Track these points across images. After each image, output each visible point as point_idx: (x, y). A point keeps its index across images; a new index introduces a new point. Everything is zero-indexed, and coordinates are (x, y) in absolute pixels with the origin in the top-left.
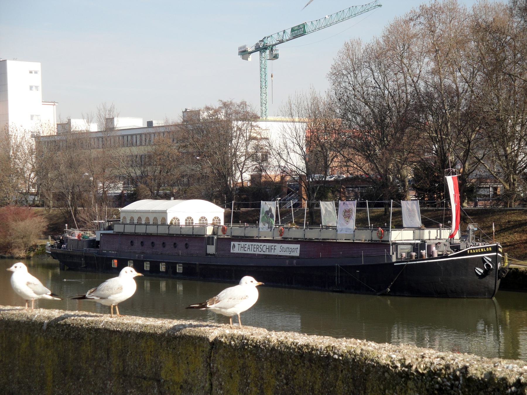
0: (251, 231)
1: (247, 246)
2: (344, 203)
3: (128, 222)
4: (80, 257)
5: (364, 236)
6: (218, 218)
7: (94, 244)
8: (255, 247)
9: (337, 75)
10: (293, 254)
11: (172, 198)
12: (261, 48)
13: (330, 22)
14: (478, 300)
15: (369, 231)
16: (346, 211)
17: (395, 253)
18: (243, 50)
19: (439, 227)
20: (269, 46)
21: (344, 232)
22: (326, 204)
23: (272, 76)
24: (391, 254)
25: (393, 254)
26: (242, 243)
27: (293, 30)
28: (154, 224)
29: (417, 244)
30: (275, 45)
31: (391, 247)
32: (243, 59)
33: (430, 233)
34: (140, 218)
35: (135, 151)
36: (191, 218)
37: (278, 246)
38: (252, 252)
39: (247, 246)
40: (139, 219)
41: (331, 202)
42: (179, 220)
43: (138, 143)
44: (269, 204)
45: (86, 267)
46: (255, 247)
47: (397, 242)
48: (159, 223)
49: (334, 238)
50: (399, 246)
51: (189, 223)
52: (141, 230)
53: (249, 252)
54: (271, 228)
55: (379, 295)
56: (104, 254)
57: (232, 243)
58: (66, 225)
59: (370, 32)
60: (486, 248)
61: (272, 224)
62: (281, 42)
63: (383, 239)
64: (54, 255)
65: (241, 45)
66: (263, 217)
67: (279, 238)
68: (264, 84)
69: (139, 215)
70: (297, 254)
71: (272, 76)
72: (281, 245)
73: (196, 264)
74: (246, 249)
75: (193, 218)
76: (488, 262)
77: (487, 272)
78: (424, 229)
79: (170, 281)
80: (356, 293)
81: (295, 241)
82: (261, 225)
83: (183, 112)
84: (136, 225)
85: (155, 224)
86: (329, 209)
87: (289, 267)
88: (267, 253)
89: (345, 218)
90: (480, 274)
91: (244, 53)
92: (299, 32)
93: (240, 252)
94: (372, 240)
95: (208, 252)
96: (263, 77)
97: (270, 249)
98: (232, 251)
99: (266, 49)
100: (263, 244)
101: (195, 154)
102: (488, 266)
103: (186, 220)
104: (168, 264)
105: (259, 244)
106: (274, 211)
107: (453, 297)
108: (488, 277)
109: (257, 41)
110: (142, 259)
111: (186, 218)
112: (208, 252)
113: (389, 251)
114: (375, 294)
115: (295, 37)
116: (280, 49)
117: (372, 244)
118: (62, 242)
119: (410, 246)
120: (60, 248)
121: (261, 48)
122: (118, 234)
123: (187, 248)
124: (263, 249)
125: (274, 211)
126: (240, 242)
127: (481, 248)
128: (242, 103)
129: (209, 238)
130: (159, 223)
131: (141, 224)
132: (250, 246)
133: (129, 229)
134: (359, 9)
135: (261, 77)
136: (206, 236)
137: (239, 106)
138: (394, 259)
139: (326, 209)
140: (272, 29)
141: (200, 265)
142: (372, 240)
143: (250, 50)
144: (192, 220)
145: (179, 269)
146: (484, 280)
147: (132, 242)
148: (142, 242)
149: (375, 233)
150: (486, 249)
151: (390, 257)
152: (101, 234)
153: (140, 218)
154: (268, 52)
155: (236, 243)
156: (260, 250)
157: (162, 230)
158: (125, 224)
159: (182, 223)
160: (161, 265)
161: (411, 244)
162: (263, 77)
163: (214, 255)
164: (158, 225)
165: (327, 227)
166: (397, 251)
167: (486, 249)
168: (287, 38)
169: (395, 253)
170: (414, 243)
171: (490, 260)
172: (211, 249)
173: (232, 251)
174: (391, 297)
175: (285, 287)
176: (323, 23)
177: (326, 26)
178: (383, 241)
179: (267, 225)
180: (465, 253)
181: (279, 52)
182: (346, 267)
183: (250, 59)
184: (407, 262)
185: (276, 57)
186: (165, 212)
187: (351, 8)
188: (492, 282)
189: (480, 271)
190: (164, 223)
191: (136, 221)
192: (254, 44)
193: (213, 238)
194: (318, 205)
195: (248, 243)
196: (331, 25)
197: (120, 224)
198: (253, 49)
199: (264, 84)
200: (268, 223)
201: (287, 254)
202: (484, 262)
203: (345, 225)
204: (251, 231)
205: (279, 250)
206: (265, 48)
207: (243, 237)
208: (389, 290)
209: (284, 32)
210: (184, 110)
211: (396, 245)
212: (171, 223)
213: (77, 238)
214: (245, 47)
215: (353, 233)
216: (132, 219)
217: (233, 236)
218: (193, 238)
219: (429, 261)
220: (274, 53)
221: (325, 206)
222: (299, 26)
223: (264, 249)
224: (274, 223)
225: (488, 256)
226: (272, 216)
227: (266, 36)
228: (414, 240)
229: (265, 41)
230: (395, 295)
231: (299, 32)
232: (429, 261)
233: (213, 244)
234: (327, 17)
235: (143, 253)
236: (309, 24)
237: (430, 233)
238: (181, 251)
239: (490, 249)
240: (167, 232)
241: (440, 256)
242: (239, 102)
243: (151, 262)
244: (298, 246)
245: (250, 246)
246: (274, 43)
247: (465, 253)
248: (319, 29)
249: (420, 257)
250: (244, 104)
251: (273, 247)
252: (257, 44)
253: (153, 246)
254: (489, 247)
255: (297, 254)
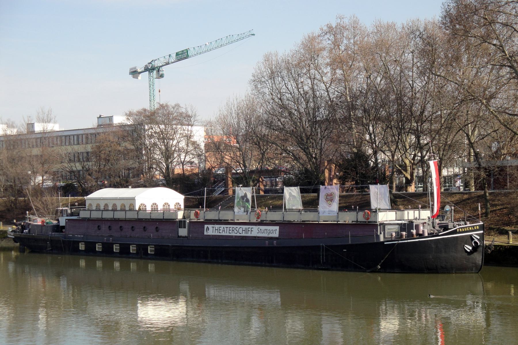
0: (226, 215)
1: (221, 229)
2: (325, 188)
3: (94, 208)
4: (45, 241)
5: (348, 217)
6: (179, 203)
7: (58, 228)
8: (250, 229)
9: (257, 81)
10: (271, 235)
11: (130, 187)
12: (150, 69)
13: (210, 48)
14: (467, 275)
15: (355, 213)
16: (328, 195)
17: (382, 233)
18: (134, 70)
19: (418, 208)
20: (157, 67)
21: (326, 214)
22: (290, 190)
23: (159, 92)
24: (379, 234)
25: (381, 233)
26: (217, 226)
27: (177, 54)
28: (121, 210)
29: (405, 224)
30: (162, 66)
31: (379, 227)
32: (134, 77)
33: (408, 213)
34: (106, 205)
35: (80, 148)
36: (156, 204)
37: (255, 228)
38: (228, 234)
39: (221, 229)
40: (106, 205)
41: (296, 188)
42: (145, 206)
43: (84, 141)
44: (244, 190)
45: (52, 250)
46: (231, 229)
47: (385, 222)
48: (127, 208)
49: (315, 220)
50: (386, 226)
51: (155, 208)
52: (108, 215)
53: (223, 234)
54: (247, 212)
55: (369, 272)
56: (70, 237)
57: (206, 226)
58: (28, 212)
59: (286, 45)
60: (473, 227)
61: (248, 207)
62: (168, 64)
63: (369, 220)
64: (15, 240)
65: (132, 66)
66: (238, 202)
67: (254, 220)
68: (152, 98)
69: (106, 202)
70: (276, 235)
71: (159, 92)
72: (259, 227)
73: (168, 246)
74: (220, 231)
75: (157, 204)
76: (476, 240)
77: (475, 248)
78: (403, 211)
79: (142, 262)
80: (343, 271)
81: (273, 223)
82: (236, 209)
83: (98, 118)
84: (103, 211)
85: (123, 210)
86: (293, 194)
87: (269, 247)
88: (244, 234)
89: (327, 201)
90: (469, 251)
91: (135, 73)
92: (182, 55)
93: (214, 234)
94: (357, 221)
95: (180, 234)
96: (152, 92)
97: (246, 231)
98: (205, 233)
99: (154, 69)
100: (239, 226)
101: (119, 152)
102: (475, 243)
103: (152, 206)
104: (87, 244)
105: (235, 226)
106: (249, 196)
107: (443, 273)
108: (475, 254)
109: (146, 64)
110: (111, 241)
111: (163, 203)
112: (180, 234)
113: (377, 231)
114: (365, 271)
115: (179, 60)
116: (165, 70)
117: (357, 225)
118: (23, 227)
119: (397, 226)
120: (22, 232)
121: (150, 69)
122: (84, 220)
123: (157, 231)
124: (239, 231)
125: (249, 196)
126: (214, 225)
127: (469, 227)
128: (176, 105)
129: (180, 221)
130: (127, 208)
131: (108, 210)
132: (226, 229)
133: (96, 215)
134: (236, 37)
135: (150, 92)
136: (177, 220)
137: (173, 108)
138: (382, 239)
139: (290, 194)
140: (157, 55)
141: (173, 246)
142: (357, 221)
143: (139, 71)
144: (157, 206)
145: (98, 247)
146: (472, 256)
147: (99, 226)
148: (110, 227)
149: (361, 214)
150: (474, 228)
151: (378, 237)
152: (66, 219)
153: (106, 205)
154: (155, 72)
155: (210, 226)
156: (236, 232)
157: (131, 215)
158: (91, 211)
159: (149, 208)
160: (131, 247)
161: (398, 224)
162: (152, 92)
163: (186, 237)
164: (126, 211)
165: (291, 210)
166: (384, 230)
167: (474, 228)
168: (173, 61)
169: (382, 233)
170: (401, 224)
171: (478, 237)
172: (183, 232)
173: (205, 233)
174: (382, 274)
175: (265, 266)
176: (204, 48)
177: (208, 51)
178: (369, 222)
179: (243, 209)
180: (455, 232)
181: (164, 72)
182: (332, 247)
183: (140, 78)
184: (398, 241)
185: (162, 76)
186: (133, 199)
187: (228, 37)
188: (478, 258)
189: (468, 248)
190: (132, 209)
191: (102, 208)
192: (144, 65)
193: (185, 222)
194: (369, 188)
195: (222, 226)
196: (211, 50)
197: (86, 210)
198: (143, 69)
199: (152, 98)
200: (244, 207)
201: (265, 235)
202: (472, 239)
203: (328, 207)
204: (226, 215)
205: (256, 232)
206: (153, 69)
207: (217, 220)
208: (379, 267)
209: (170, 55)
210: (99, 116)
211: (383, 225)
212: (140, 209)
213: (40, 224)
214: (135, 68)
215: (336, 215)
216: (98, 206)
217: (206, 220)
218: (164, 222)
219: (409, 241)
220: (160, 73)
221: (290, 191)
222: (183, 51)
223: (238, 231)
224: (250, 207)
225: (476, 234)
226: (247, 201)
227: (154, 59)
228: (396, 220)
229: (153, 63)
230: (385, 272)
231: (182, 55)
232: (409, 241)
233: (185, 227)
234: (207, 44)
235: (111, 236)
236: (192, 49)
237: (408, 213)
238: (152, 233)
239: (478, 227)
240: (136, 217)
241: (431, 235)
242: (173, 105)
243: (121, 245)
244: (277, 228)
245: (226, 229)
246: (161, 65)
247: (455, 232)
248: (200, 53)
249: (410, 236)
250: (178, 106)
251: (250, 229)
252: (146, 66)
253: (121, 230)
254: (476, 226)
255: (276, 235)
